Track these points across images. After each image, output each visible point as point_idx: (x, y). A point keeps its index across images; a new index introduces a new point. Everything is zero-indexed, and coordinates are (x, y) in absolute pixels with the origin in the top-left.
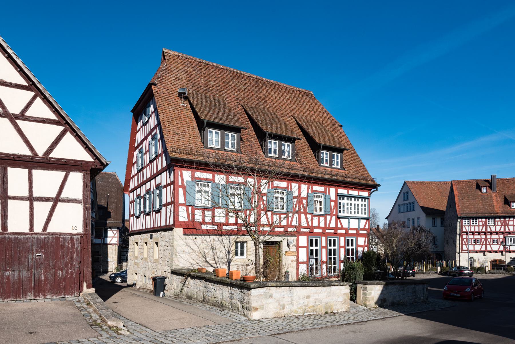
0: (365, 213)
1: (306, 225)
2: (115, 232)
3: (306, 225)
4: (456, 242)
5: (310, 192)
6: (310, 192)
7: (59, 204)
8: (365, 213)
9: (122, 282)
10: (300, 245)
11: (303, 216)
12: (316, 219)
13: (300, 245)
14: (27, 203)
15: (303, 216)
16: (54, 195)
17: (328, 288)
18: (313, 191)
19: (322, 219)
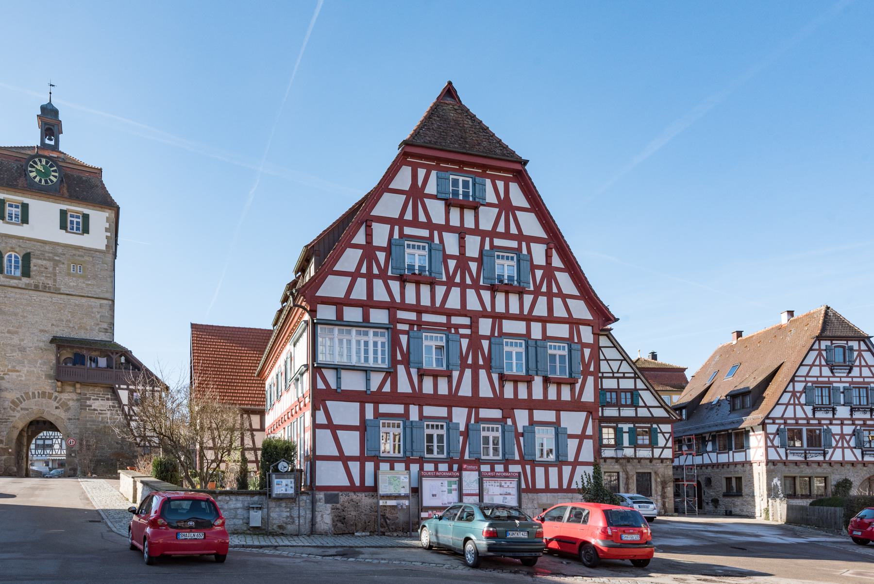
0: (399, 452)
1: (350, 463)
2: (759, 437)
3: (350, 463)
4: (808, 439)
5: (473, 421)
6: (473, 421)
7: (335, 422)
8: (399, 452)
9: (801, 439)
10: (357, 433)
11: (483, 373)
12: (540, 471)
13: (357, 433)
14: (579, 433)
15: (483, 373)
16: (336, 421)
17: (32, 419)
18: (478, 420)
19: (553, 472)
